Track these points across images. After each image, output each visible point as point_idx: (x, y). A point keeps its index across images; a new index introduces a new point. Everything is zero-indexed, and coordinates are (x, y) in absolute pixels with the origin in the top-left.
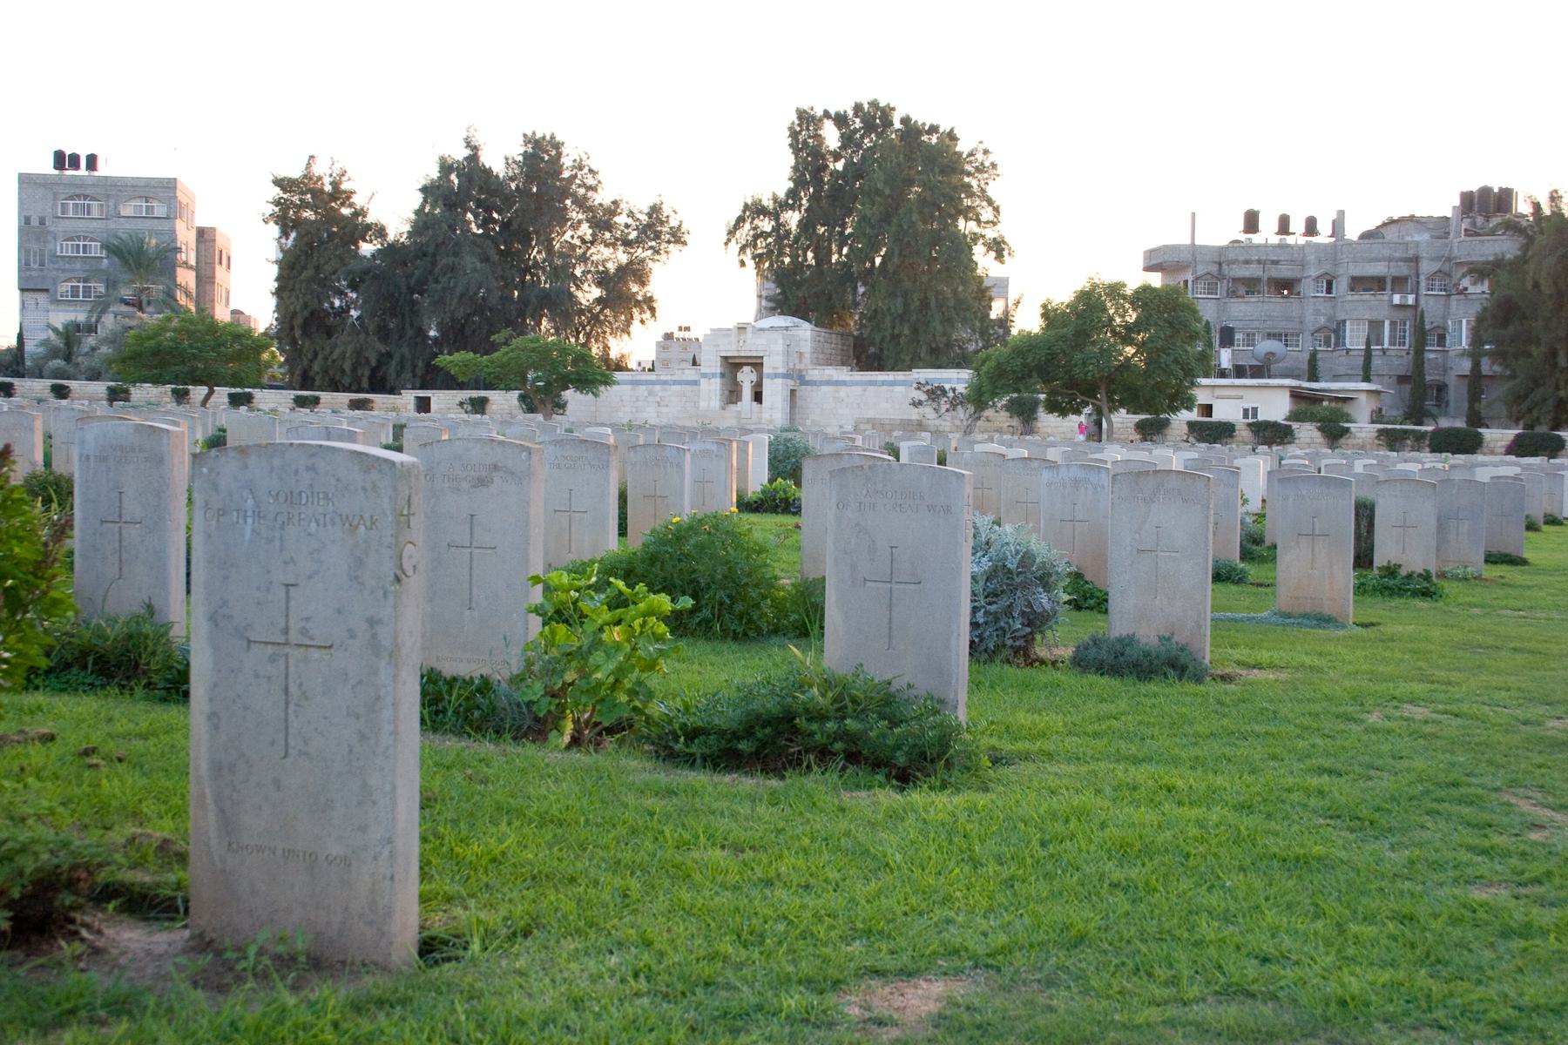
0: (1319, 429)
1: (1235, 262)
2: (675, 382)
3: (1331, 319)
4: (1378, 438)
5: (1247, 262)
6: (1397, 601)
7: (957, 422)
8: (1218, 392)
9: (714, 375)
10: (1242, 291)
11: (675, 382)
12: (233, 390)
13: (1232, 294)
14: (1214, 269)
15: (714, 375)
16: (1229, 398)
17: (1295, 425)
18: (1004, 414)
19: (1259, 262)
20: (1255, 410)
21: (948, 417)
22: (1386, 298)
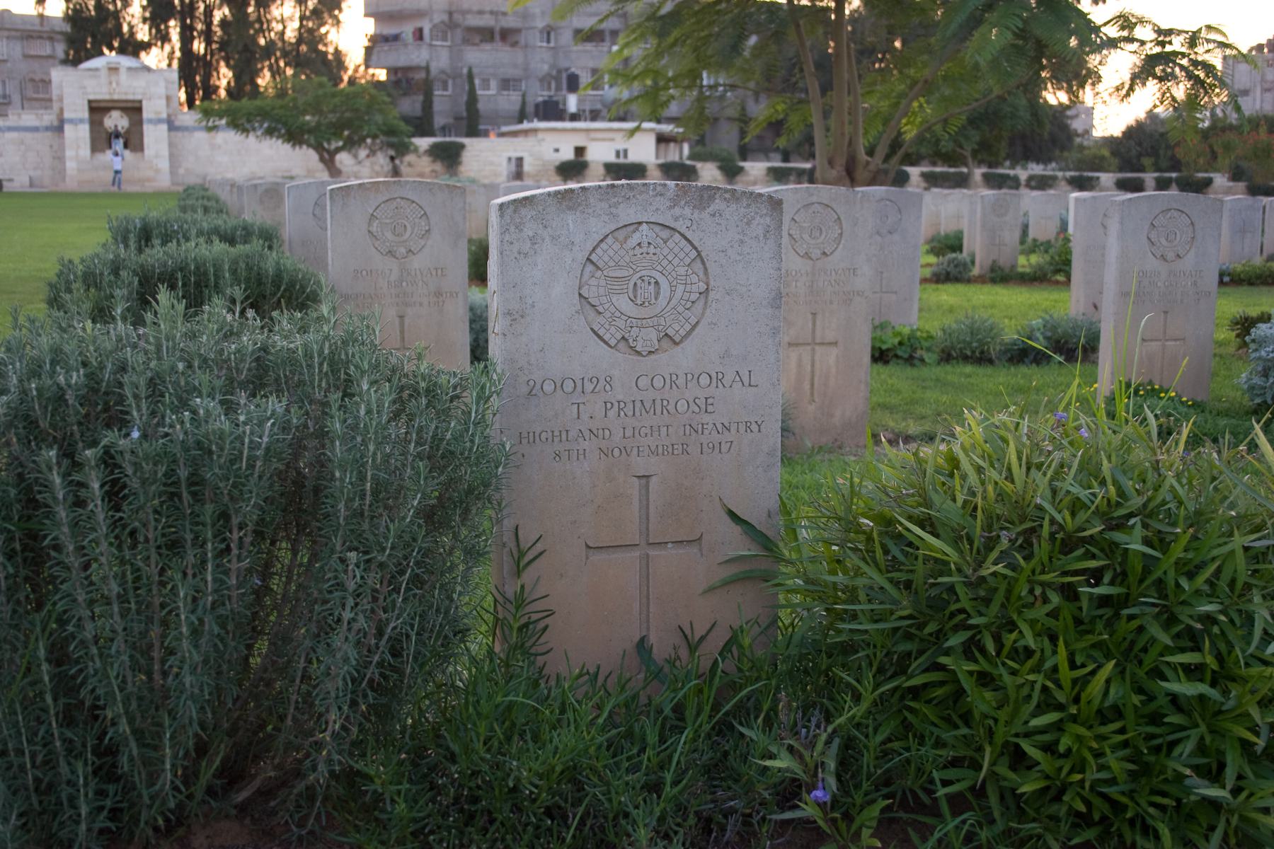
0: (720, 168)
1: (469, 12)
2: (10, 129)
3: (552, 66)
4: (768, 174)
5: (481, 12)
6: (1255, 290)
7: (377, 168)
8: (593, 135)
9: (81, 121)
10: (477, 40)
11: (10, 129)
12: (1120, 175)
13: (466, 41)
14: (445, 17)
15: (81, 121)
16: (604, 140)
17: (699, 165)
18: (426, 160)
19: (492, 13)
20: (626, 151)
21: (367, 163)
22: (605, 49)
